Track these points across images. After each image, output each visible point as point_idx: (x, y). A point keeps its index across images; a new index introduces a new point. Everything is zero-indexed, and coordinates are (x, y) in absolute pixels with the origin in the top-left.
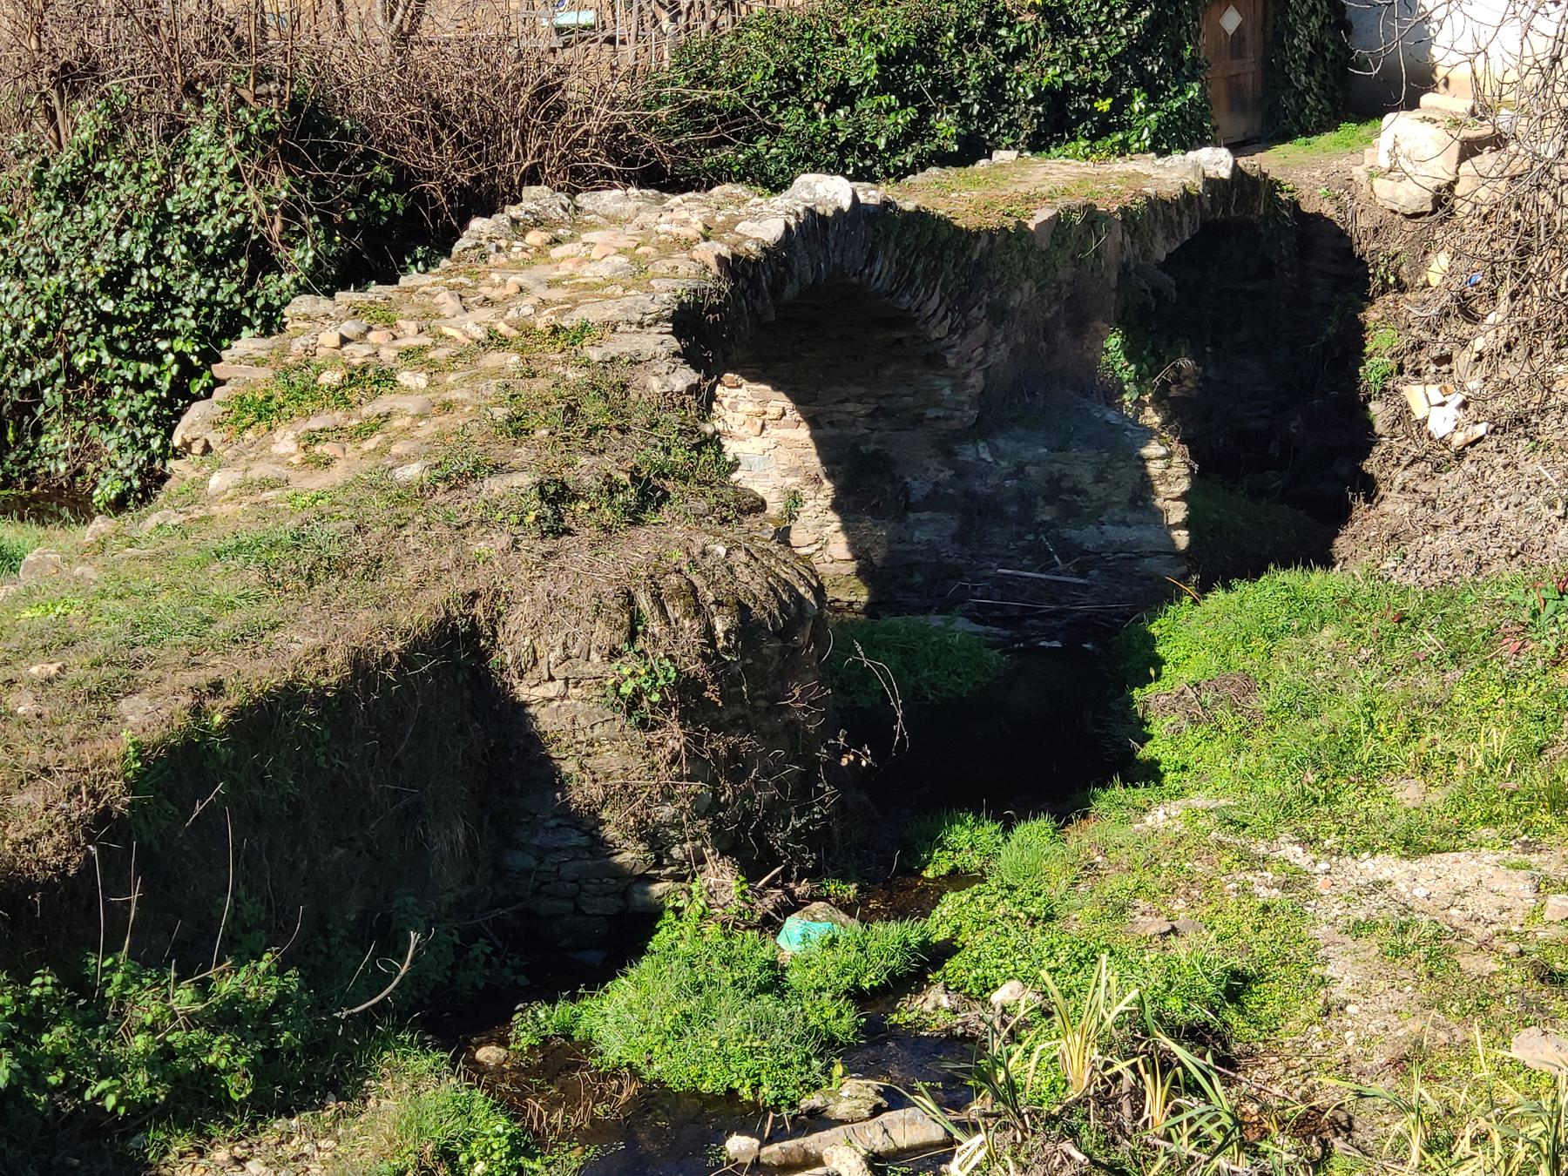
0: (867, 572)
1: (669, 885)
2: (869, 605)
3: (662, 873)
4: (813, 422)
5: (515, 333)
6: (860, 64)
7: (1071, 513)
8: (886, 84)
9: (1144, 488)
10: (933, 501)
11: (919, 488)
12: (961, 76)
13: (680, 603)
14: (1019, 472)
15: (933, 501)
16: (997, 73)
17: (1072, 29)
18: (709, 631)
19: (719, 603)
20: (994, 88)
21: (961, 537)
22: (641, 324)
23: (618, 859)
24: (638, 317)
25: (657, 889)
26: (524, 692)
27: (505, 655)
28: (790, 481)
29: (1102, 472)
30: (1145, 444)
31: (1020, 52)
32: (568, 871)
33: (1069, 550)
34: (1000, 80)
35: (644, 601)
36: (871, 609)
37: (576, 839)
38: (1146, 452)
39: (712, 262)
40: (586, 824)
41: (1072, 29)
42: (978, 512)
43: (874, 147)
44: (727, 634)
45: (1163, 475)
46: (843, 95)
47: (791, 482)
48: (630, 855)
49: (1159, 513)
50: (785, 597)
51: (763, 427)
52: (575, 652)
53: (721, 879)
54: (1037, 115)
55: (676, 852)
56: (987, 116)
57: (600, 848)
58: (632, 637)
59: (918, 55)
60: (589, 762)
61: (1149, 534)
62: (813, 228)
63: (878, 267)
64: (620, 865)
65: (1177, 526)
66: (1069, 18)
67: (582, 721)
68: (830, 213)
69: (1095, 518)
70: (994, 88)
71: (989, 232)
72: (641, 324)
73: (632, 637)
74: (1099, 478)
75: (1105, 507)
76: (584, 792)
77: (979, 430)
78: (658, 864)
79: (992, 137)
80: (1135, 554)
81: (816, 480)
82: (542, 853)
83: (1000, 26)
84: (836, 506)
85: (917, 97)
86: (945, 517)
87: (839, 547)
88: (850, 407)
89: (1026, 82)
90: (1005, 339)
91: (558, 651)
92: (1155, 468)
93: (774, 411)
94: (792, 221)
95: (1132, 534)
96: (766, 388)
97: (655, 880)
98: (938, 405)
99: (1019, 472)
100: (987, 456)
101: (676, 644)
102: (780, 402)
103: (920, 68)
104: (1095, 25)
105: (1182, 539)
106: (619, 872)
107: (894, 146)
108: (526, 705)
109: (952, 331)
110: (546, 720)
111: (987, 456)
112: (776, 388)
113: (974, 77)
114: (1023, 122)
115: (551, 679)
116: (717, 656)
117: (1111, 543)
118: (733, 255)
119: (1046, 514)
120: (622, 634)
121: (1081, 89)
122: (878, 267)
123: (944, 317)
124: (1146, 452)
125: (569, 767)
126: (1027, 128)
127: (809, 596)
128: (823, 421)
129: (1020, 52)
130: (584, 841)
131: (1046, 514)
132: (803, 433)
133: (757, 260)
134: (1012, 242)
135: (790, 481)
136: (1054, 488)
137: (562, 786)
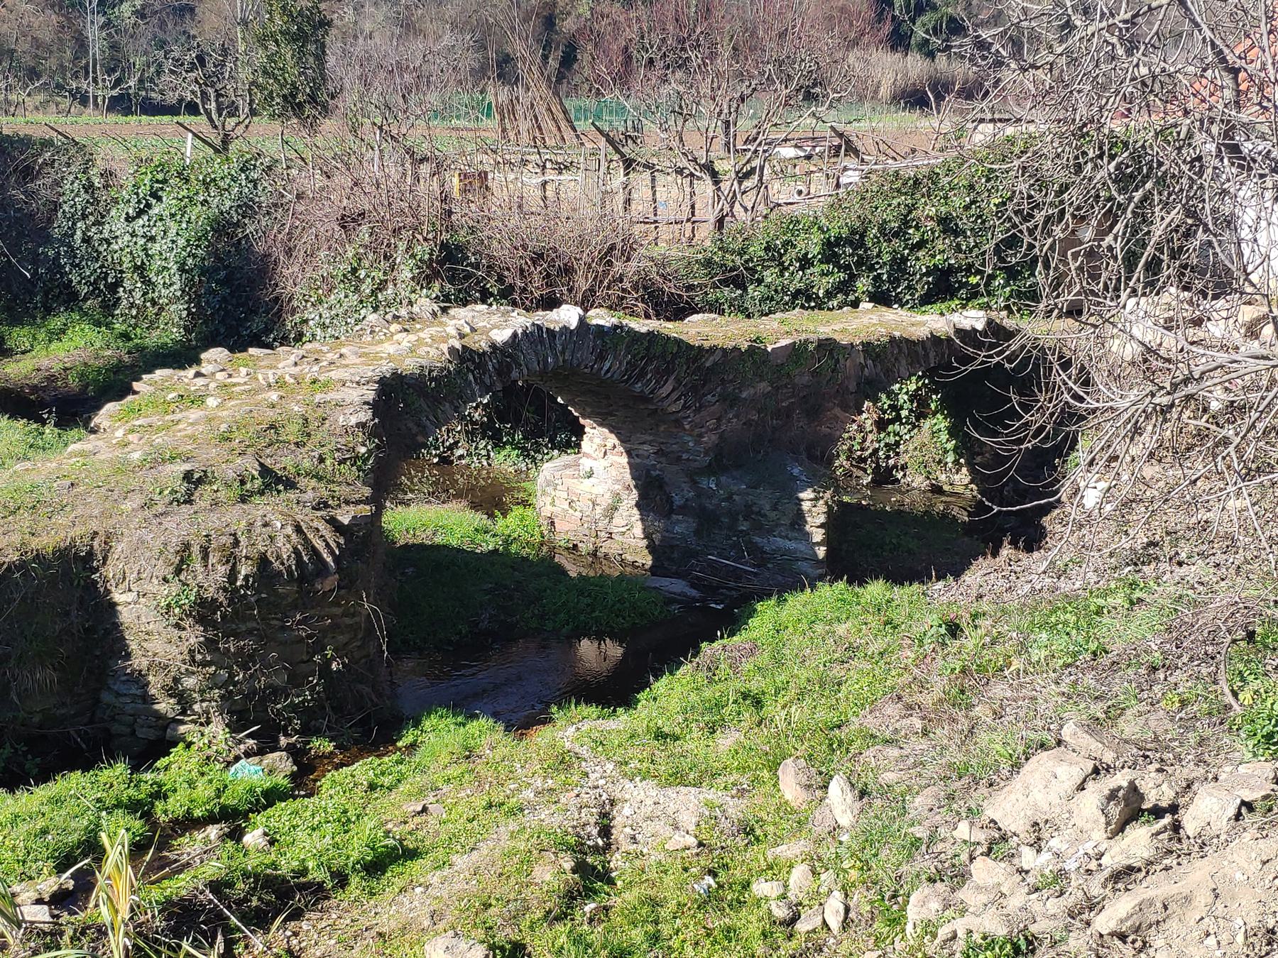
0: (651, 548)
1: (191, 726)
2: (652, 567)
3: (187, 719)
4: (629, 453)
5: (292, 381)
6: (812, 245)
7: (758, 528)
8: (826, 260)
9: (799, 519)
10: (684, 509)
11: (678, 501)
12: (878, 256)
13: (218, 554)
14: (729, 498)
15: (684, 509)
16: (902, 255)
17: (956, 233)
18: (232, 575)
19: (247, 558)
20: (899, 265)
21: (697, 532)
22: (358, 383)
23: (156, 707)
24: (358, 379)
25: (182, 729)
26: (117, 597)
27: (110, 571)
28: (617, 487)
29: (776, 504)
30: (803, 490)
31: (921, 245)
32: (129, 709)
33: (755, 550)
34: (904, 260)
35: (196, 549)
36: (654, 570)
37: (134, 690)
38: (802, 495)
39: (446, 351)
40: (139, 680)
41: (956, 233)
42: (707, 519)
43: (817, 294)
44: (246, 577)
45: (810, 511)
46: (805, 262)
47: (617, 487)
48: (165, 706)
49: (808, 535)
50: (305, 559)
51: (605, 453)
52: (144, 576)
53: (218, 729)
54: (928, 283)
55: (196, 707)
56: (895, 282)
57: (148, 700)
58: (178, 571)
59: (849, 242)
60: (145, 645)
61: (802, 548)
62: (538, 338)
63: (607, 365)
64: (157, 711)
65: (818, 544)
66: (956, 225)
67: (143, 619)
68: (557, 329)
69: (770, 532)
70: (899, 265)
71: (724, 350)
72: (358, 383)
73: (178, 571)
74: (774, 508)
75: (777, 525)
76: (139, 662)
77: (710, 470)
78: (183, 713)
79: (897, 294)
80: (793, 557)
81: (628, 488)
82: (118, 695)
83: (911, 227)
84: (638, 505)
85: (847, 267)
86: (691, 520)
87: (638, 530)
88: (646, 447)
89: (921, 263)
90: (736, 416)
91: (135, 575)
92: (806, 506)
93: (609, 445)
94: (520, 331)
95: (791, 545)
96: (606, 430)
97: (182, 723)
98: (688, 451)
99: (729, 498)
100: (713, 486)
101: (210, 579)
102: (613, 440)
103: (849, 250)
104: (972, 230)
105: (821, 552)
106: (158, 716)
107: (830, 295)
108: (116, 604)
109: (685, 407)
110: (126, 615)
111: (713, 486)
112: (611, 432)
113: (886, 258)
114: (919, 287)
115: (130, 590)
116: (237, 590)
117: (779, 549)
118: (463, 347)
119: (744, 526)
120: (171, 569)
121: (960, 269)
122: (607, 365)
123: (679, 399)
124: (802, 495)
125: (133, 646)
126: (921, 290)
127: (329, 559)
128: (634, 453)
129: (921, 245)
130: (139, 692)
131: (744, 526)
132: (624, 460)
133: (484, 353)
134: (745, 357)
135: (617, 487)
136: (749, 512)
137: (128, 656)
